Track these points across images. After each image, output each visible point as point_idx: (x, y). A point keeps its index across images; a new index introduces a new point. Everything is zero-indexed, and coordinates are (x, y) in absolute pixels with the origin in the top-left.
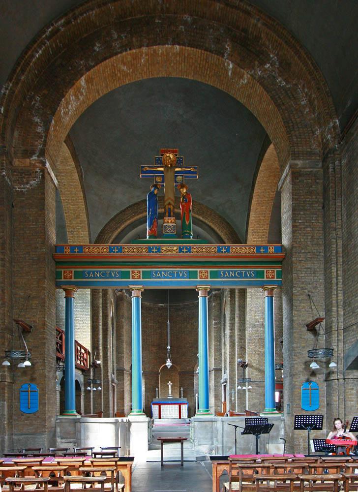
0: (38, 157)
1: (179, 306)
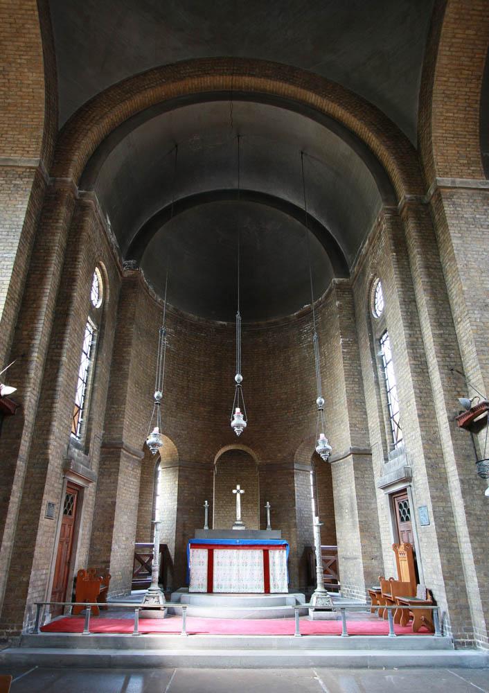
1: (258, 325)
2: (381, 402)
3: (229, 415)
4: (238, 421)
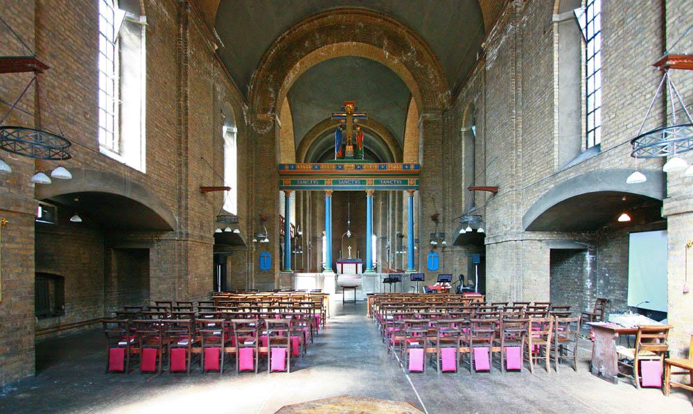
0: (272, 112)
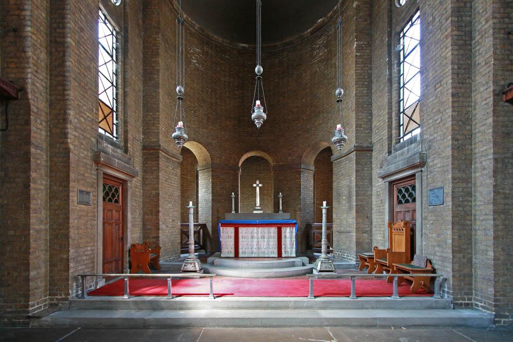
2: (391, 99)
3: (250, 110)
4: (259, 113)
